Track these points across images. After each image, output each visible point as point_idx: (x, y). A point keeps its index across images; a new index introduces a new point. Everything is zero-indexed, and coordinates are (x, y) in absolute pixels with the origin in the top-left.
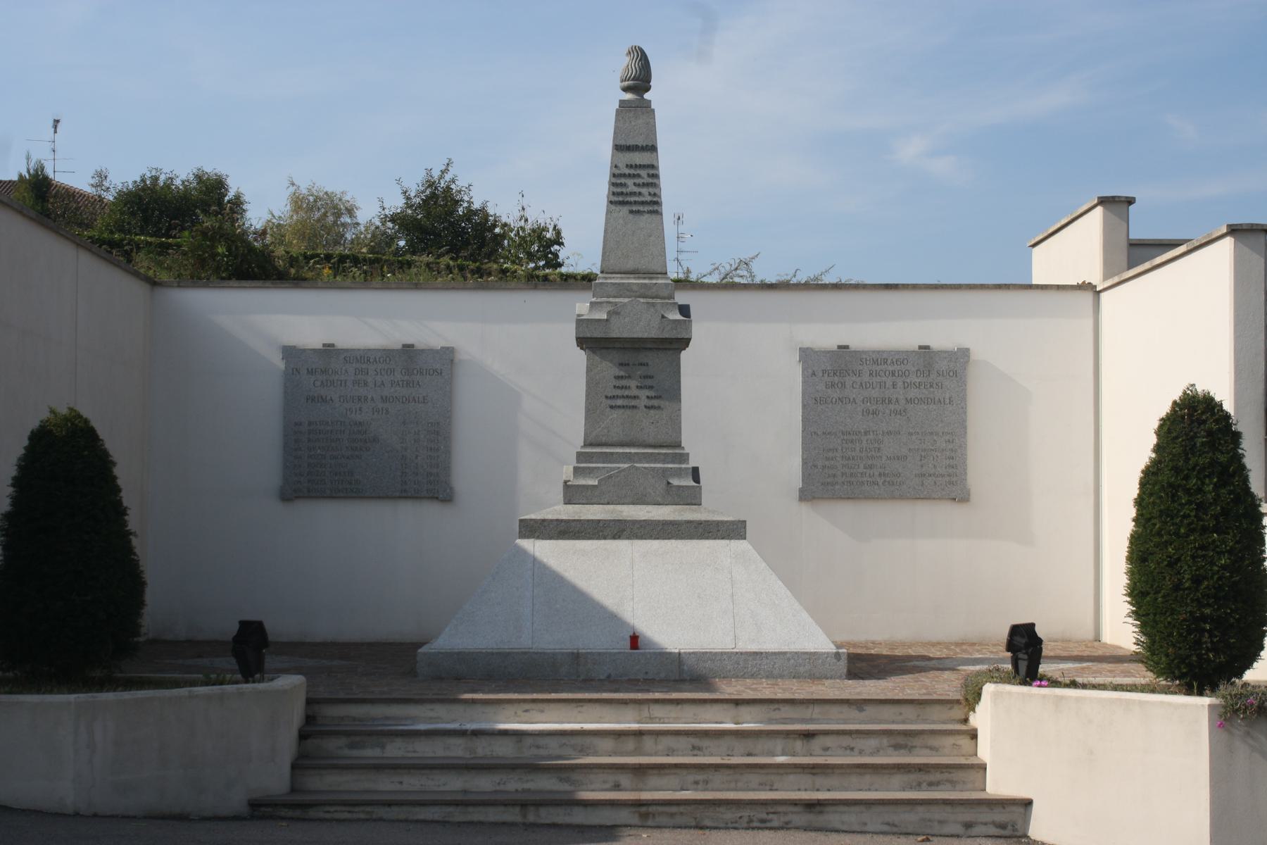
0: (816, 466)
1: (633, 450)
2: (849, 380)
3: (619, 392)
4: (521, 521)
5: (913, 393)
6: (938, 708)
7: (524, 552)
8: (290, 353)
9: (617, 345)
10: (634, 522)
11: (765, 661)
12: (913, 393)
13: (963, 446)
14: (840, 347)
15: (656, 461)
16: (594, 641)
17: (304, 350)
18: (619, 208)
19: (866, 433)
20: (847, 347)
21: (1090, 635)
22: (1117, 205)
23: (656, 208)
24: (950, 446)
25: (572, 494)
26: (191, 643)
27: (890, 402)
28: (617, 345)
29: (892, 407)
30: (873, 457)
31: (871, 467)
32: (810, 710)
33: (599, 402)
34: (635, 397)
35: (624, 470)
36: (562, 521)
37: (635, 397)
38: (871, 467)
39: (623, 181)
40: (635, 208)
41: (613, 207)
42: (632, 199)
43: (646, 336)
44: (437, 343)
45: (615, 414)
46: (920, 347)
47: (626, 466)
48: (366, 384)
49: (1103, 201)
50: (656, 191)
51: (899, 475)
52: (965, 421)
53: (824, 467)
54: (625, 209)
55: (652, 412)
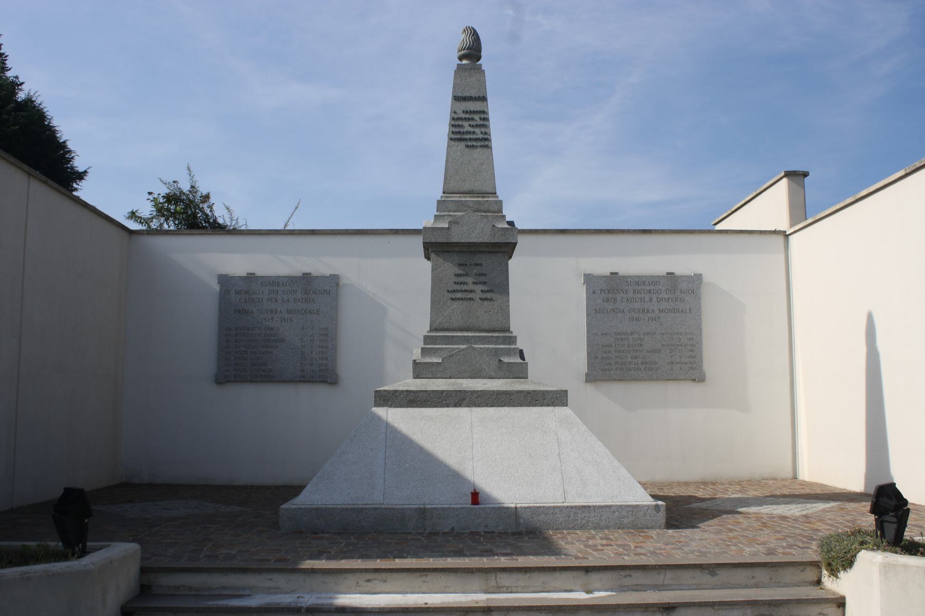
0: (597, 357)
1: (470, 334)
2: (619, 297)
3: (458, 287)
4: (376, 392)
5: (663, 305)
6: (791, 570)
7: (379, 418)
8: (224, 280)
9: (457, 249)
10: (473, 392)
11: (592, 514)
12: (663, 305)
13: (700, 342)
14: (611, 273)
15: (489, 343)
16: (439, 497)
17: (233, 277)
18: (457, 143)
19: (632, 333)
20: (617, 273)
21: (790, 475)
22: (796, 176)
23: (486, 143)
24: (691, 343)
25: (420, 370)
26: (151, 486)
27: (648, 311)
28: (457, 249)
29: (650, 315)
30: (637, 351)
31: (636, 358)
32: (662, 576)
33: (442, 294)
34: (471, 291)
35: (463, 349)
36: (411, 391)
37: (471, 291)
38: (636, 358)
39: (460, 123)
40: (470, 143)
41: (453, 143)
42: (468, 137)
43: (480, 240)
44: (327, 272)
45: (456, 305)
46: (668, 274)
47: (464, 346)
48: (276, 301)
49: (788, 174)
50: (487, 130)
51: (655, 363)
52: (700, 325)
53: (603, 358)
54: (463, 144)
55: (486, 303)
